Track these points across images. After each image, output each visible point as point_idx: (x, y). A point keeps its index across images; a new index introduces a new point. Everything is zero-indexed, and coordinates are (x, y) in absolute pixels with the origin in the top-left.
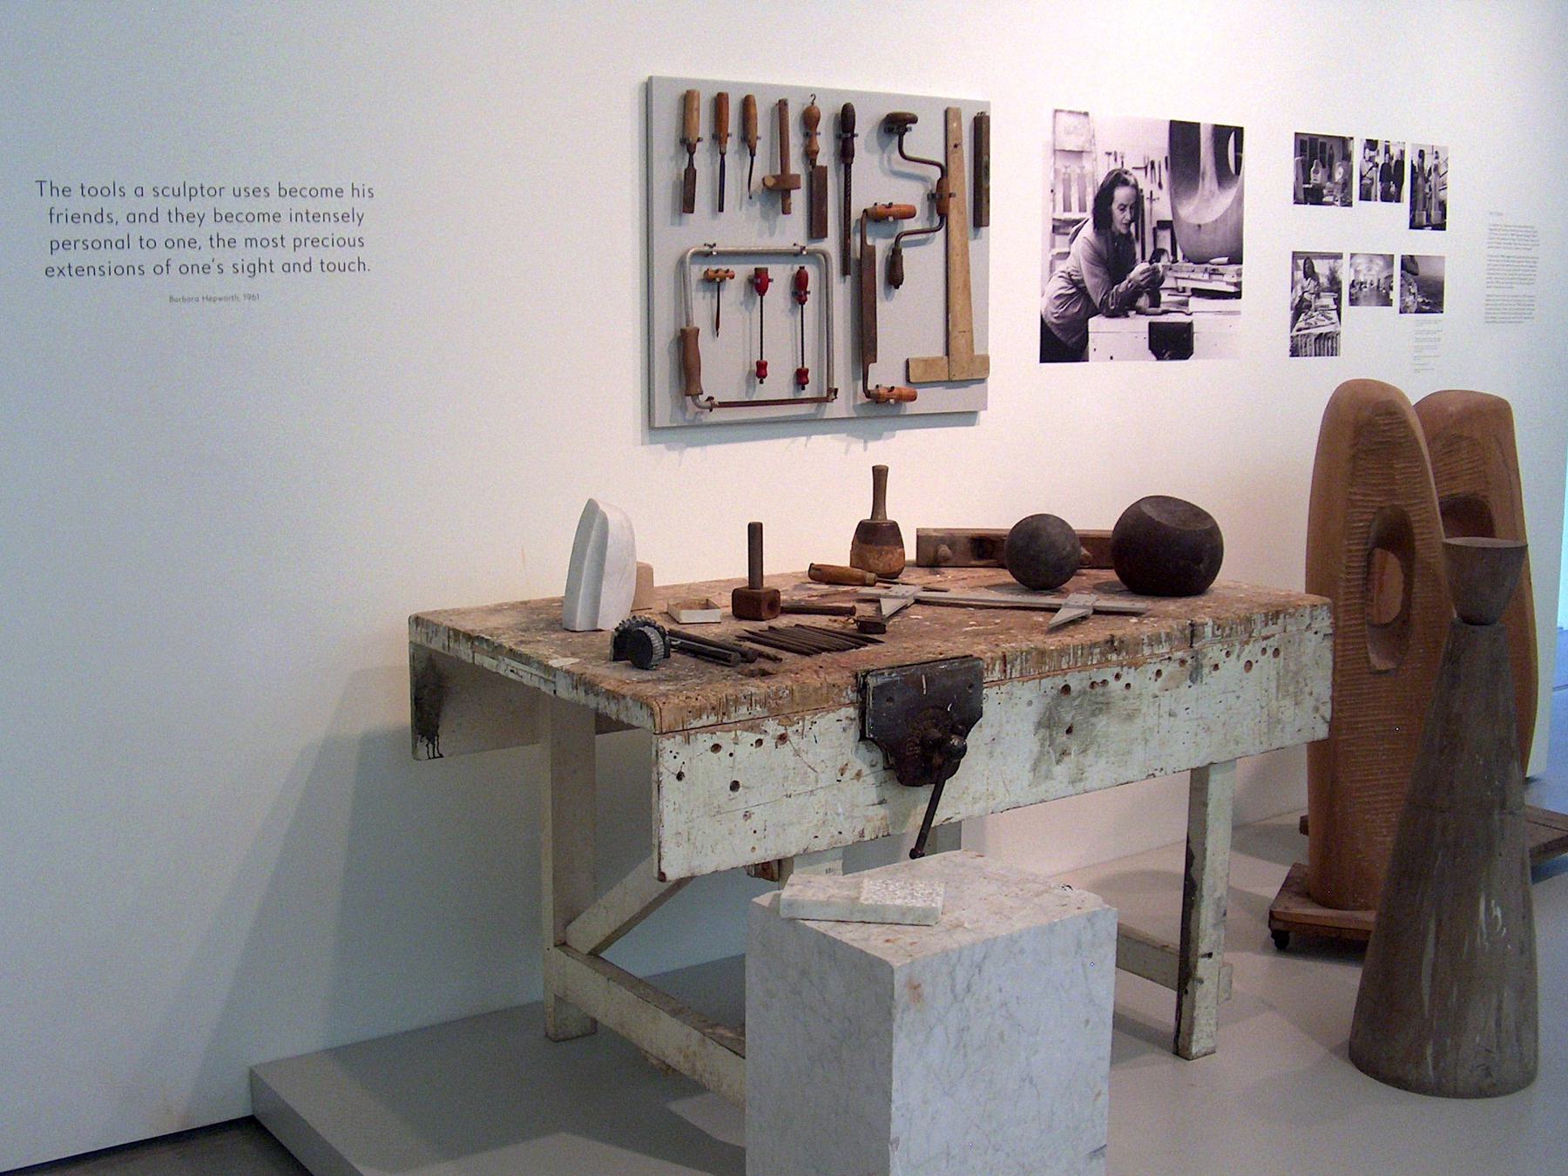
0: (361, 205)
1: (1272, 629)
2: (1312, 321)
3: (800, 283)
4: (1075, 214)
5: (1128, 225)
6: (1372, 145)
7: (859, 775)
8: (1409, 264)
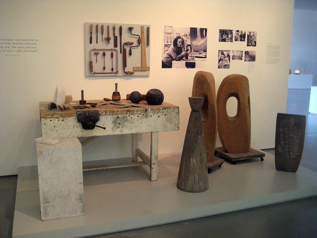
0: (36, 42)
1: (164, 111)
2: (223, 62)
3: (112, 54)
4: (169, 43)
5: (181, 45)
6: (238, 31)
7: (77, 127)
8: (247, 53)
